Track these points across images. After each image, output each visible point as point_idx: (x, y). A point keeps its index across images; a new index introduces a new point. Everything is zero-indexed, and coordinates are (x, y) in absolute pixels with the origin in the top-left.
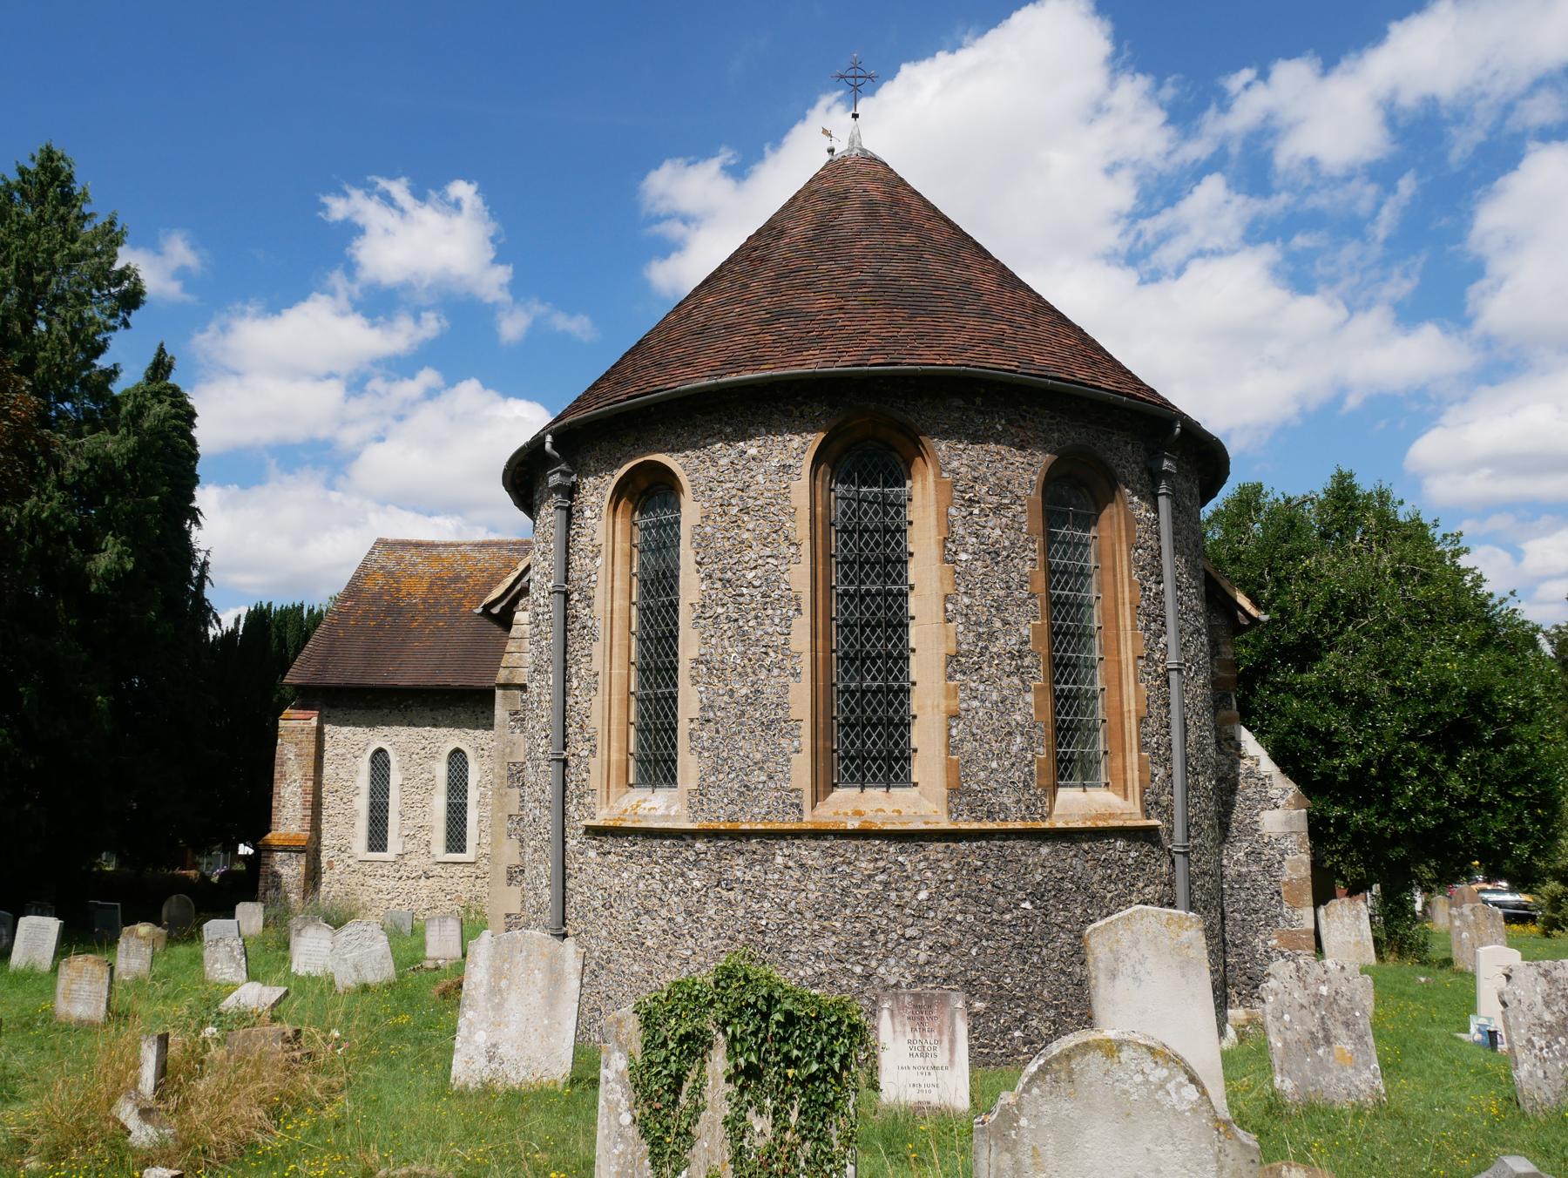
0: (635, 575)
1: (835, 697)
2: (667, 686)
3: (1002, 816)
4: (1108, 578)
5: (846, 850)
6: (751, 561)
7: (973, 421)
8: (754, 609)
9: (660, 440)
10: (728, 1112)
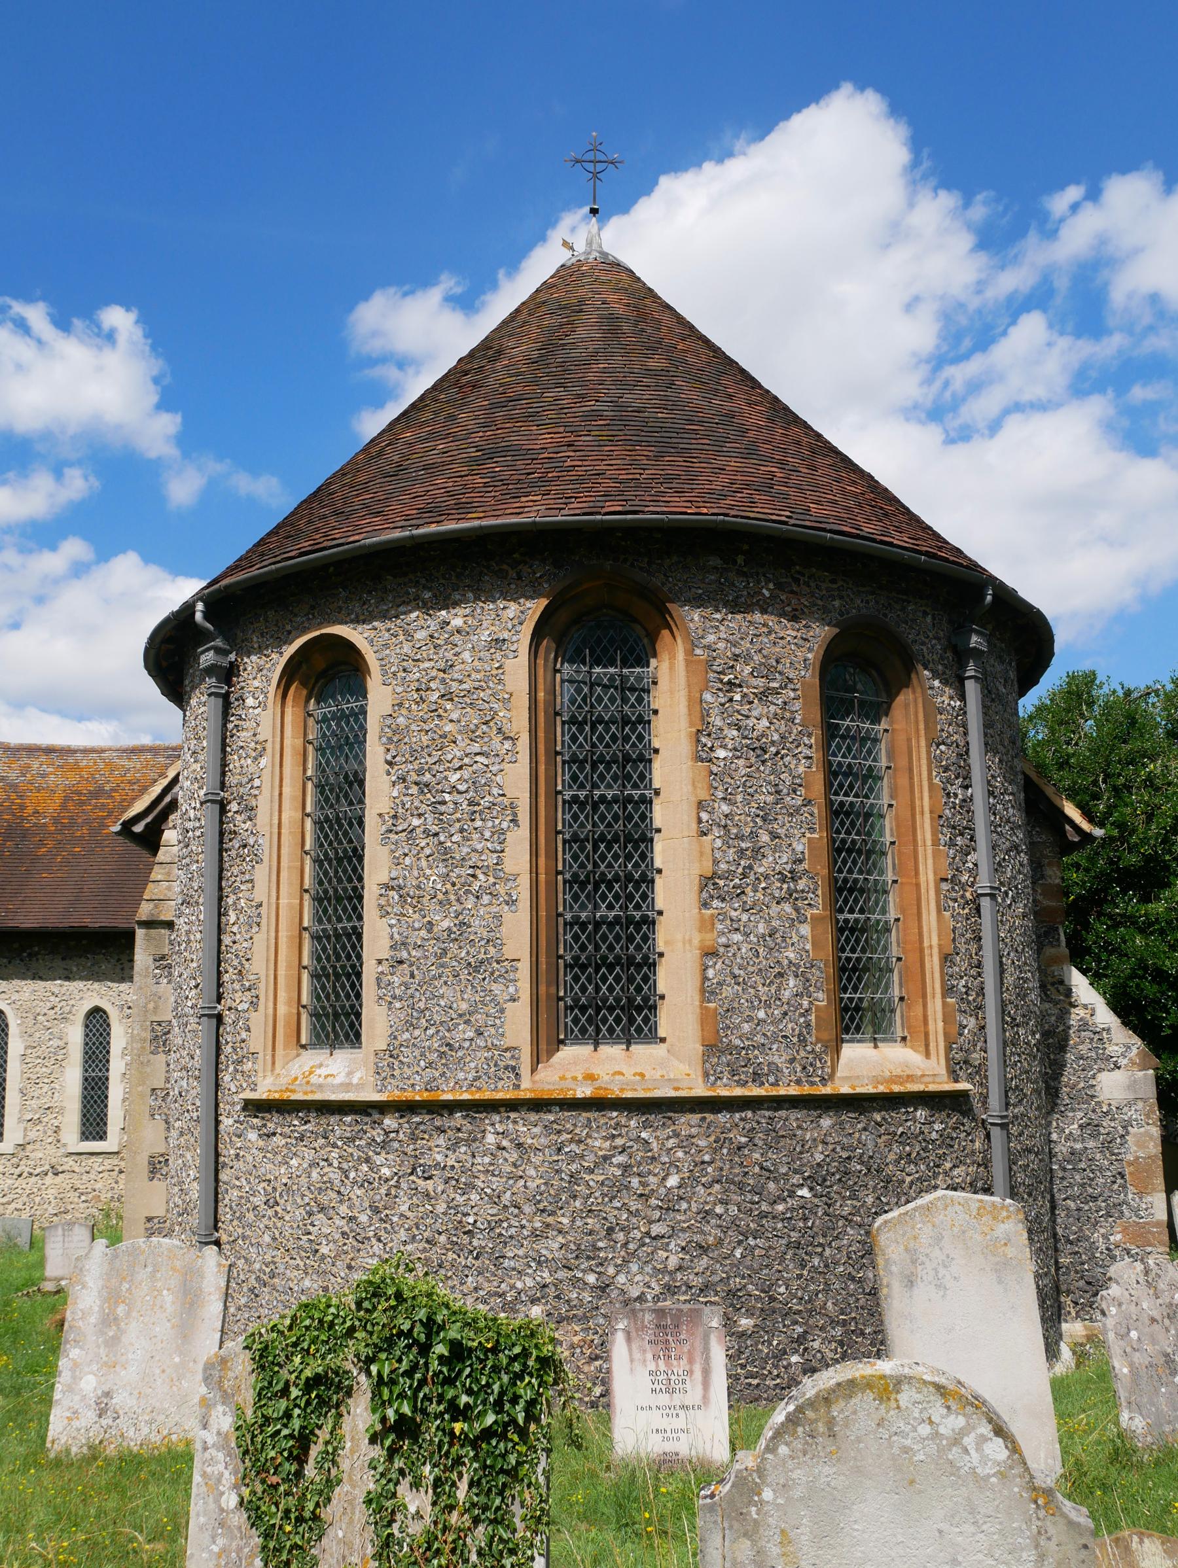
0: (309, 779)
1: (561, 931)
2: (350, 919)
3: (772, 1079)
4: (903, 781)
5: (575, 1125)
6: (456, 760)
7: (733, 585)
8: (459, 820)
9: (340, 608)
10: (372, 1486)
